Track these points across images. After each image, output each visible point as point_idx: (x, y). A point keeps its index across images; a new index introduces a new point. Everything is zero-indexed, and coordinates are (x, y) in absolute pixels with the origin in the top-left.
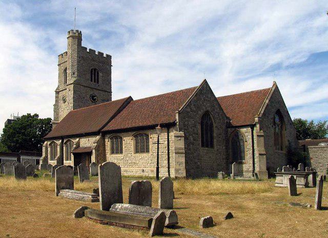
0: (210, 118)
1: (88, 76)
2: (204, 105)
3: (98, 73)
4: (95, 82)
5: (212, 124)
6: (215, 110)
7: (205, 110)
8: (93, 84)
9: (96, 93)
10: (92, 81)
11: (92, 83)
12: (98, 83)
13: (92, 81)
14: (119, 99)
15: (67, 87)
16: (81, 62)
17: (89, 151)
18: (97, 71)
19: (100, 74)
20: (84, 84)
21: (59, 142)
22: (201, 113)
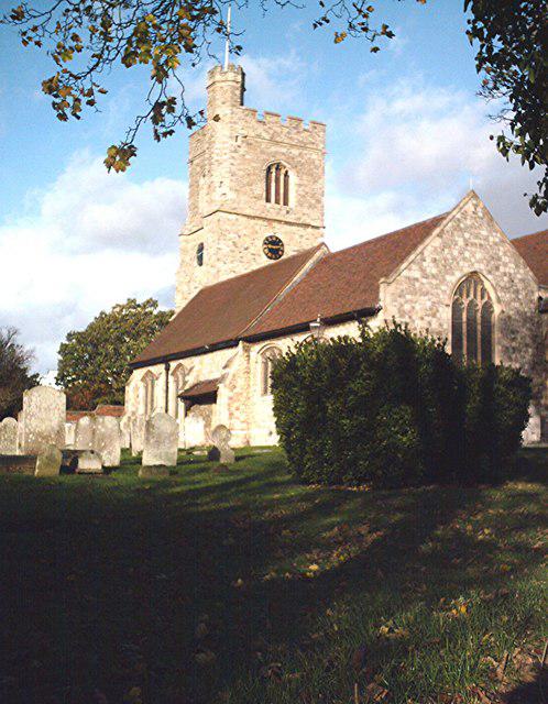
0: (484, 290)
1: (260, 188)
2: (464, 259)
3: (286, 175)
4: (277, 202)
5: (491, 306)
6: (502, 269)
7: (467, 270)
8: (272, 209)
9: (281, 232)
10: (268, 200)
11: (268, 205)
12: (286, 203)
13: (268, 200)
14: (533, 232)
15: (205, 221)
16: (242, 151)
17: (210, 389)
18: (283, 171)
19: (293, 179)
20: (248, 212)
21: (159, 369)
22: (453, 279)
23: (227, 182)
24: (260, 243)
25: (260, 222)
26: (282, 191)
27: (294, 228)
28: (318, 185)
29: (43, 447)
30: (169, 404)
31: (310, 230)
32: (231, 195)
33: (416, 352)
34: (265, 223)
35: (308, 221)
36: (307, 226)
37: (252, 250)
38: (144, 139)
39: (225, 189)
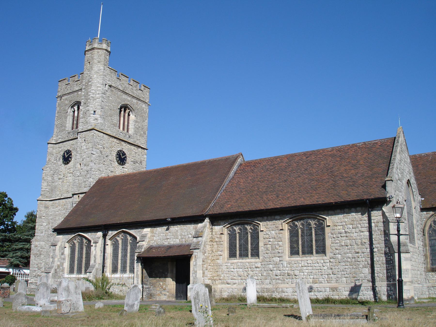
9: (126, 148)
12: (128, 131)
20: (109, 132)
23: (98, 112)
24: (114, 154)
25: (115, 140)
26: (126, 123)
27: (133, 147)
28: (29, 254)
29: (322, 297)
30: (377, 269)
31: (140, 149)
32: (100, 121)
33: (236, 296)
34: (118, 142)
35: (139, 144)
36: (139, 147)
37: (110, 158)
38: (39, 305)
39: (97, 116)
